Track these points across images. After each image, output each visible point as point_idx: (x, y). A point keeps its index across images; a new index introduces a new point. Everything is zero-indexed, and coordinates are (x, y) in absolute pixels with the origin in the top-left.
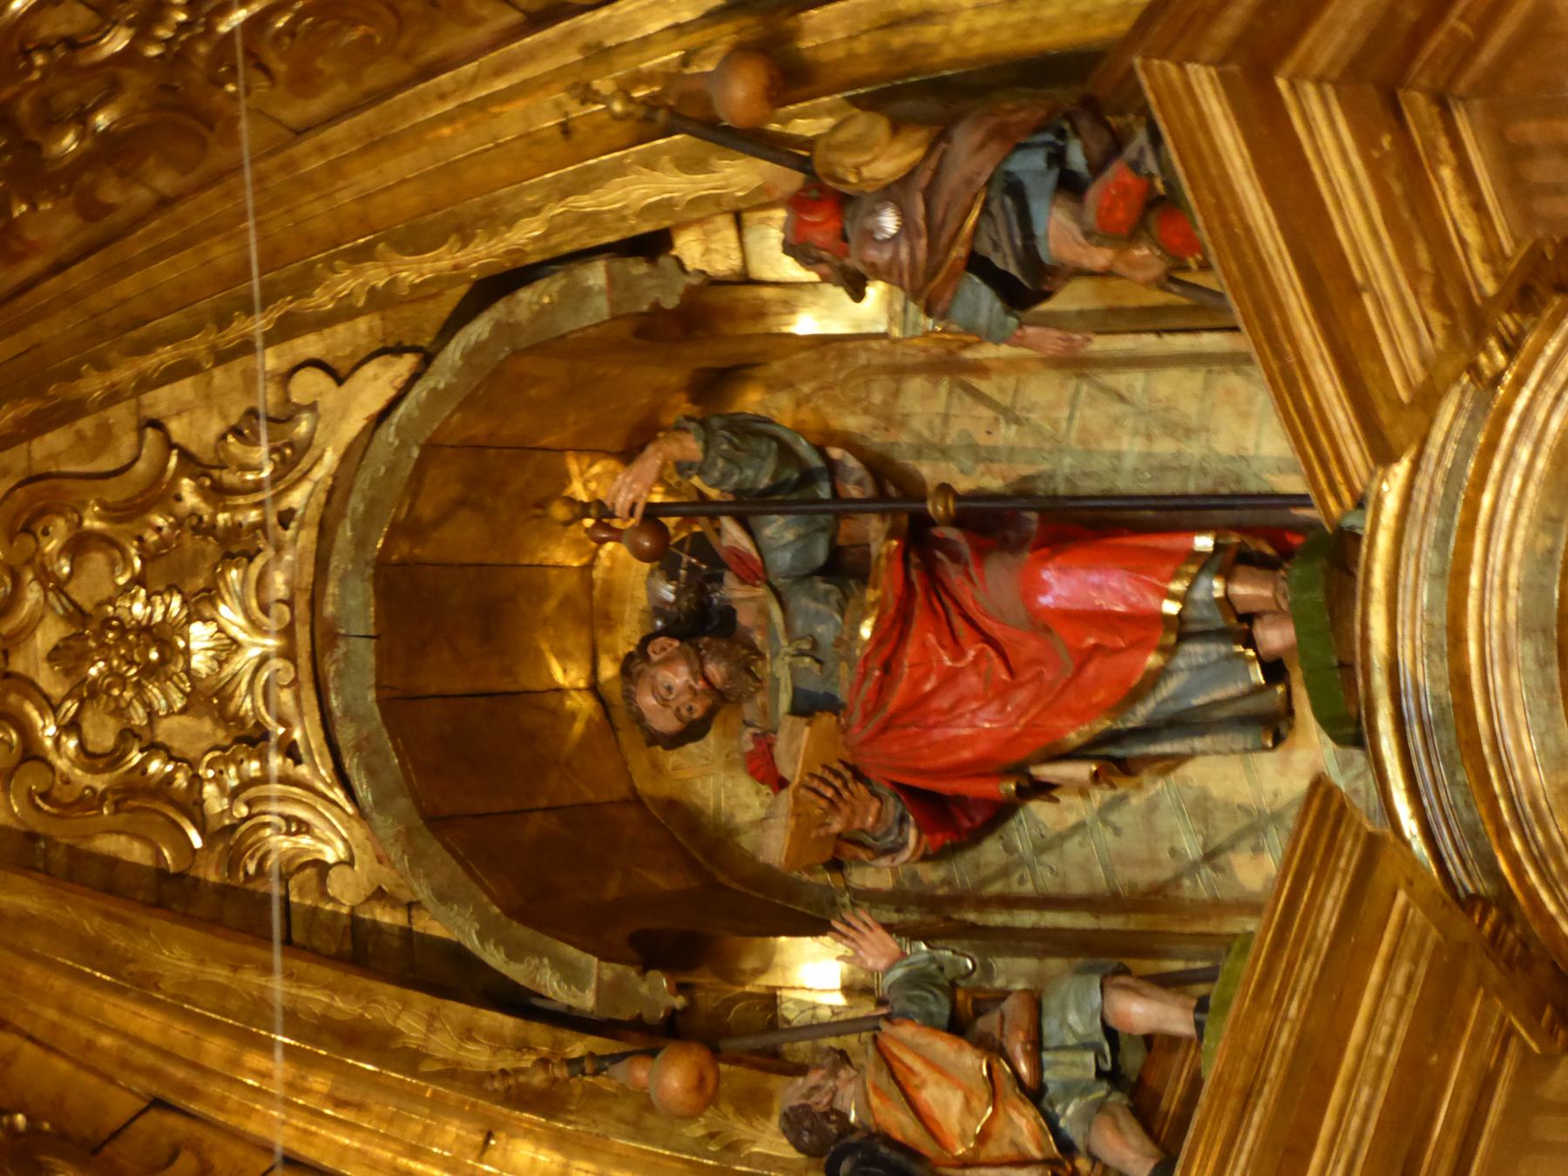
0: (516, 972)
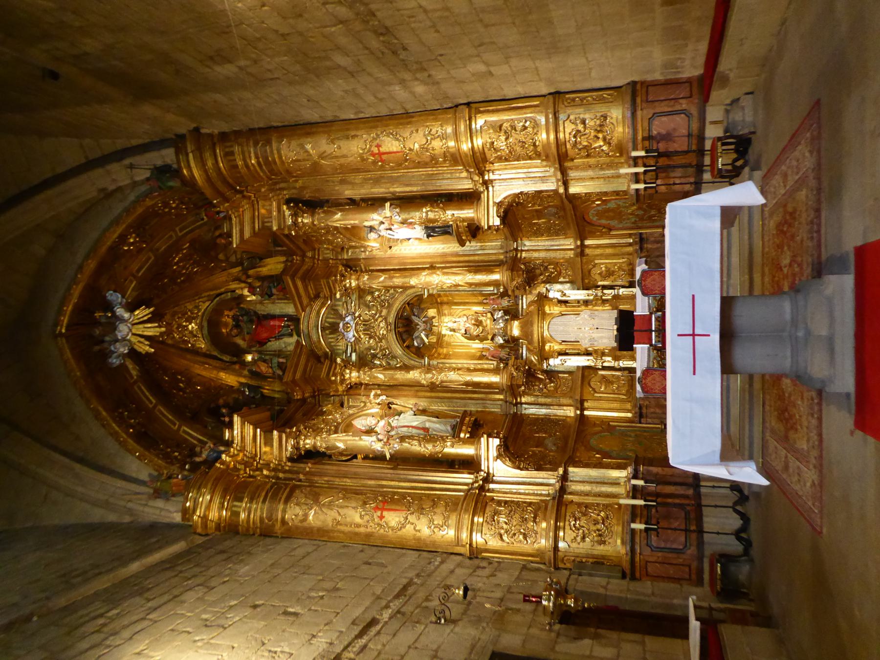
0: (221, 357)
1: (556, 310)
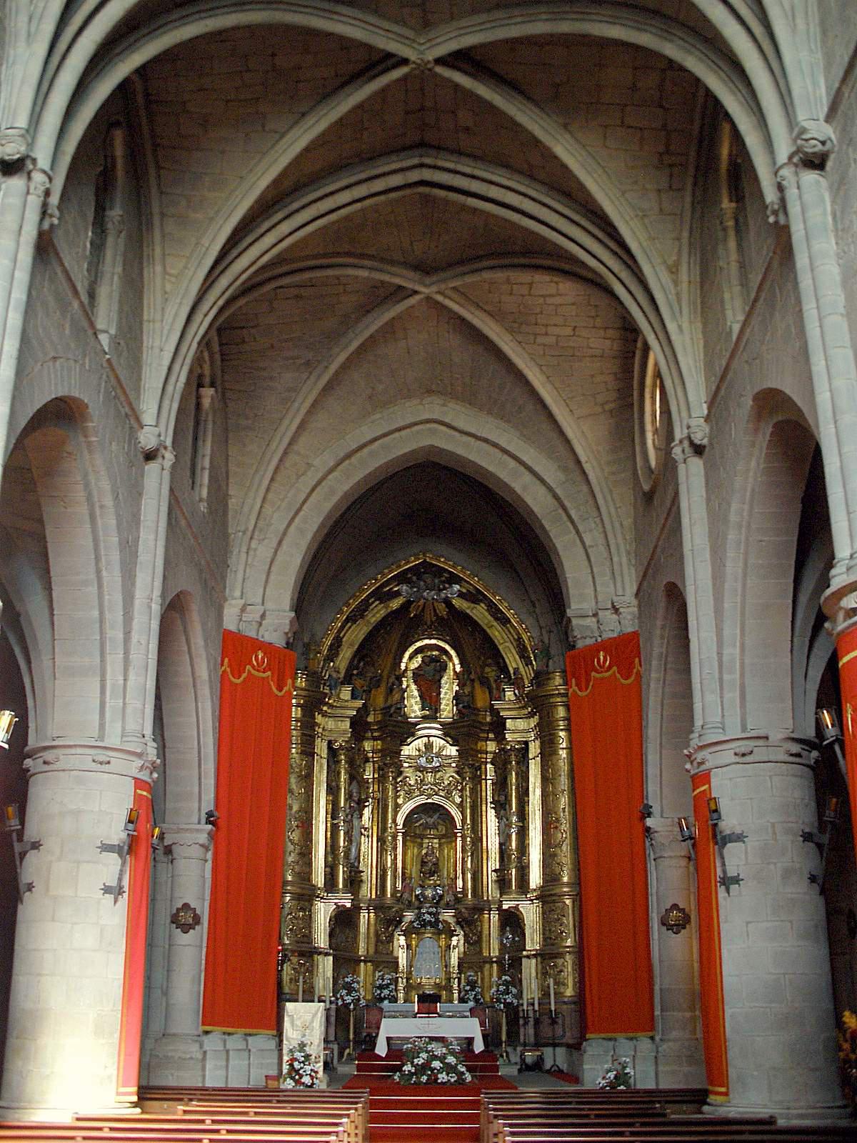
1: (443, 943)
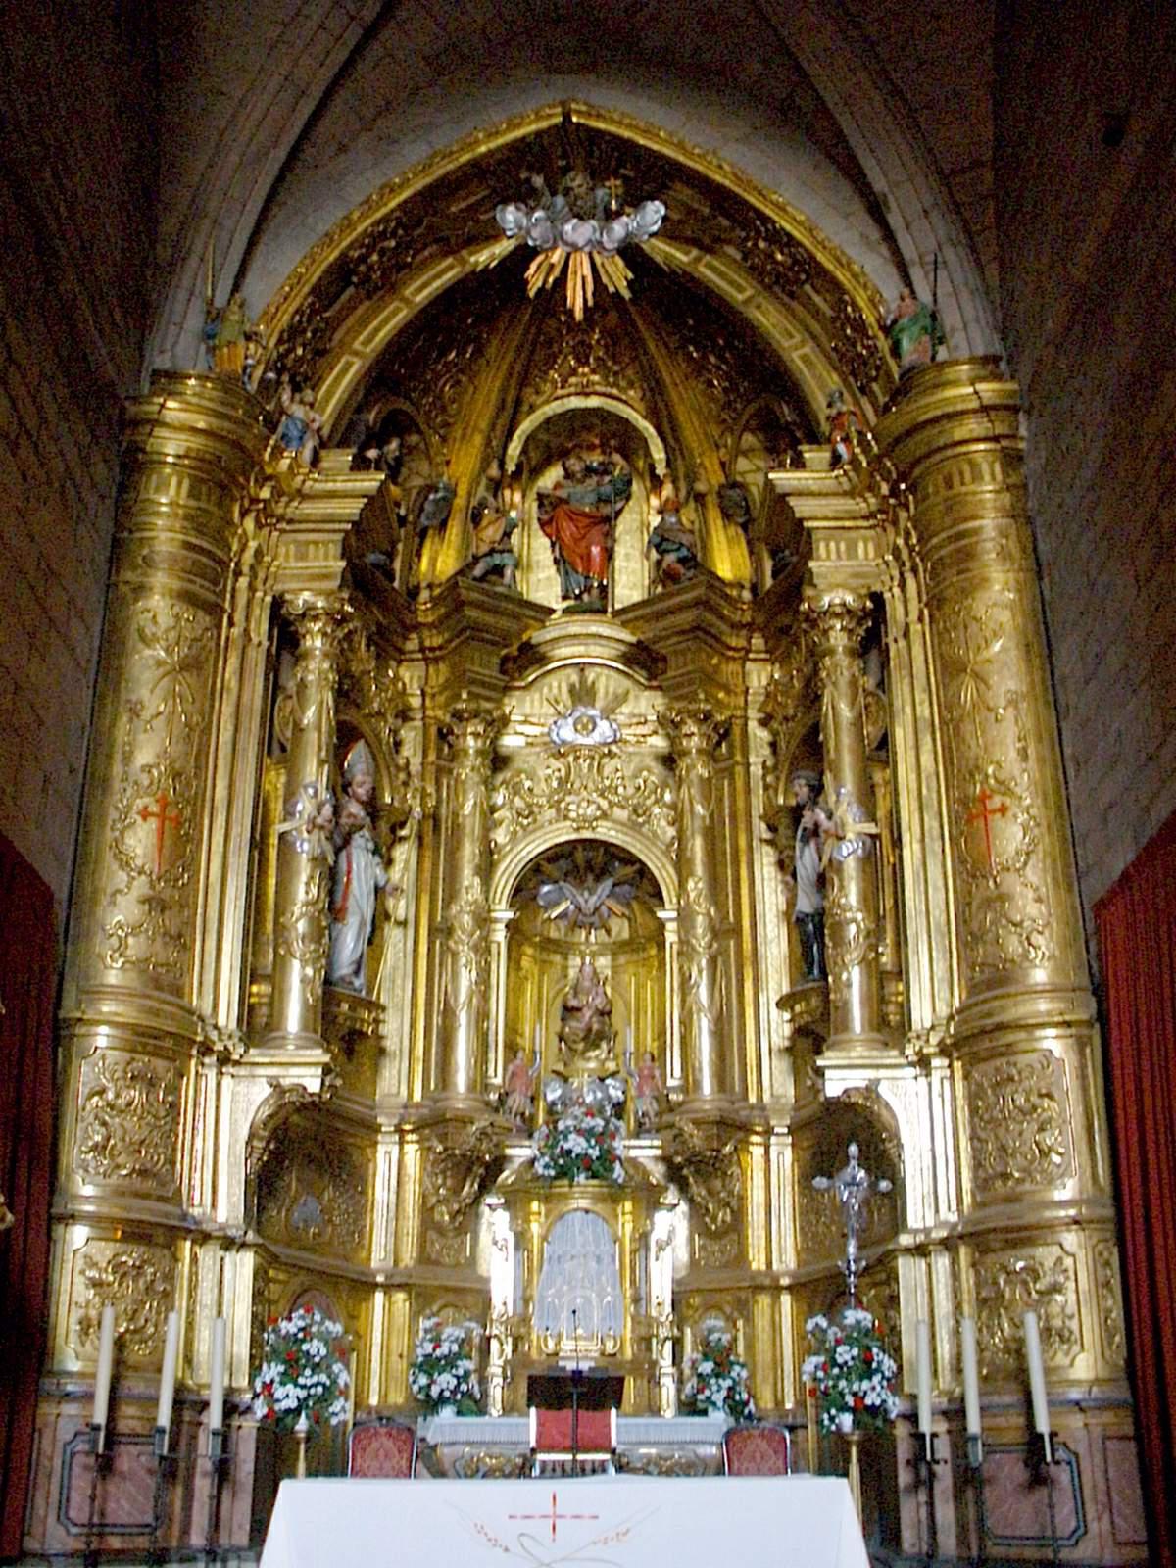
1: (626, 1226)
